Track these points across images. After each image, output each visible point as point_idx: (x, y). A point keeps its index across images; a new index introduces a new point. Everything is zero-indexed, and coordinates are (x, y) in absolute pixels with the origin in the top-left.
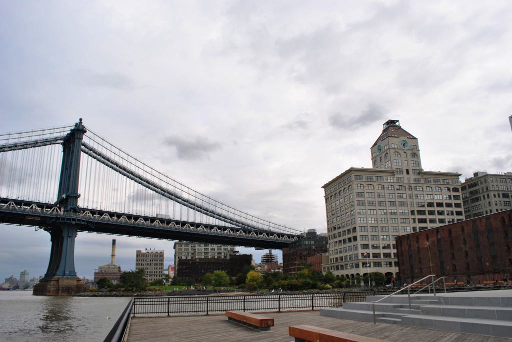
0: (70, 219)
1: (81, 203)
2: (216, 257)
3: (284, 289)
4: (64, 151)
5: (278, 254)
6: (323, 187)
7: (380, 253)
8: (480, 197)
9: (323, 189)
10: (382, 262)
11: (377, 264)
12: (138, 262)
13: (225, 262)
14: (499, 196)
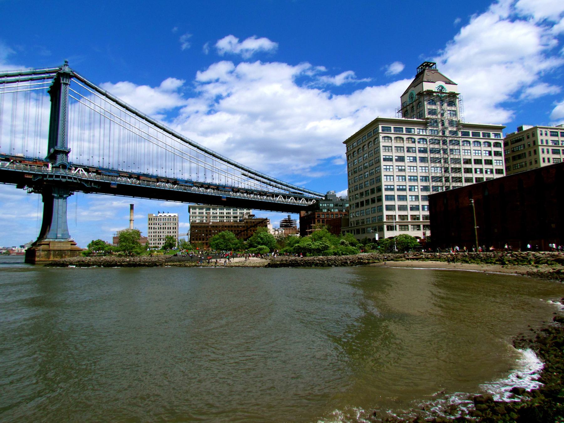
0: (66, 176)
1: (72, 157)
2: (232, 221)
3: (104, 266)
4: (52, 100)
5: (296, 217)
6: (344, 143)
7: (407, 216)
8: (525, 153)
9: (345, 145)
10: (410, 226)
11: (404, 227)
12: (151, 226)
13: (494, 296)
14: (548, 152)
